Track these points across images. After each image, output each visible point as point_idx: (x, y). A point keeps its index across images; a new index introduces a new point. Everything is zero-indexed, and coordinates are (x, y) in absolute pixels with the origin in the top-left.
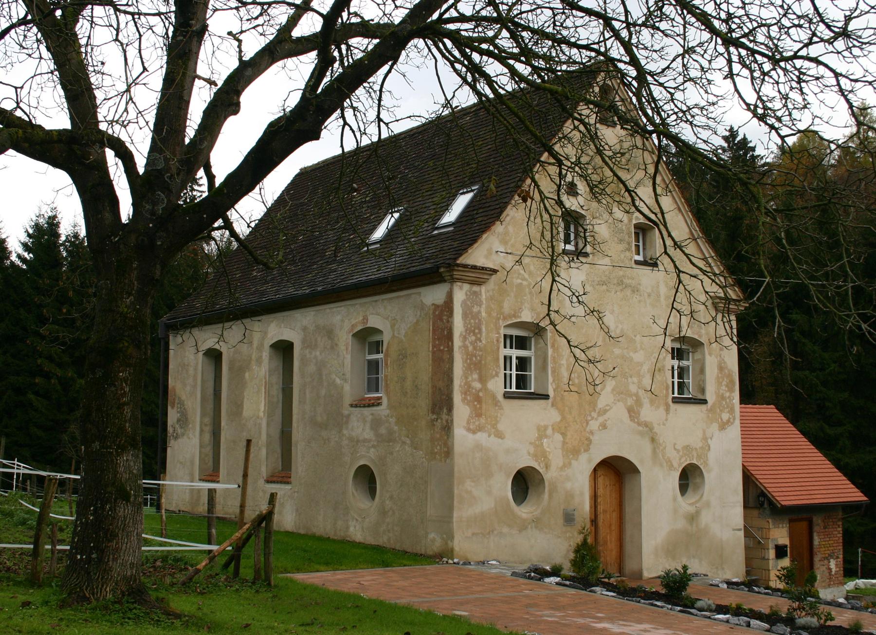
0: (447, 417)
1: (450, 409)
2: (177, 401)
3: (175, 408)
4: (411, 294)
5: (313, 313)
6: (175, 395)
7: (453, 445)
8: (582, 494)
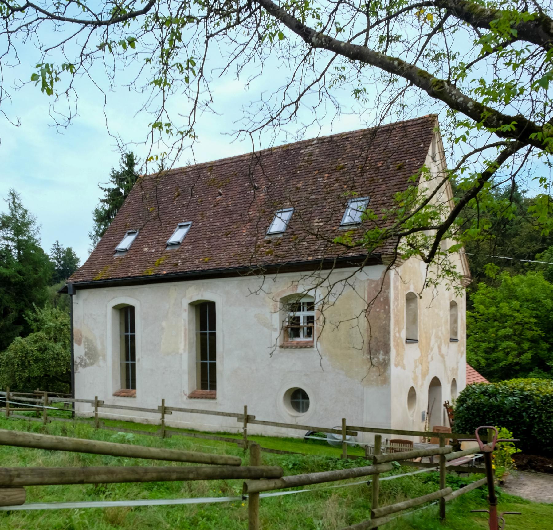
0: (384, 357)
1: (387, 351)
2: (83, 340)
3: (82, 345)
4: (343, 272)
5: (236, 282)
6: (81, 335)
7: (390, 376)
8: (213, 467)
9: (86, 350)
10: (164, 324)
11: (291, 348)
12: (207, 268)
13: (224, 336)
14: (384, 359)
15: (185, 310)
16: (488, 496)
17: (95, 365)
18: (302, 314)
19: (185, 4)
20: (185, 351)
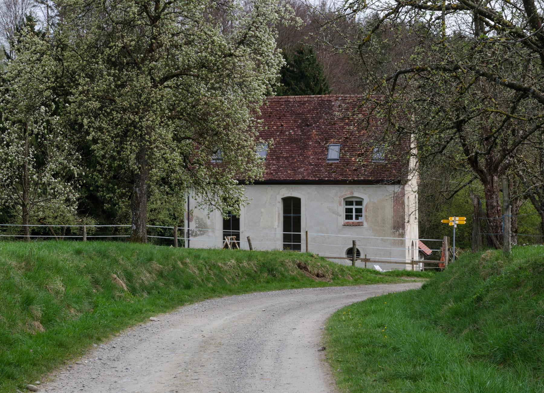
5: (315, 188)
9: (197, 225)
10: (263, 210)
11: (350, 226)
12: (297, 179)
13: (306, 218)
14: (402, 232)
15: (279, 202)
16: (53, 109)
17: (205, 236)
18: (354, 207)
19: (1, 146)
20: (278, 227)
